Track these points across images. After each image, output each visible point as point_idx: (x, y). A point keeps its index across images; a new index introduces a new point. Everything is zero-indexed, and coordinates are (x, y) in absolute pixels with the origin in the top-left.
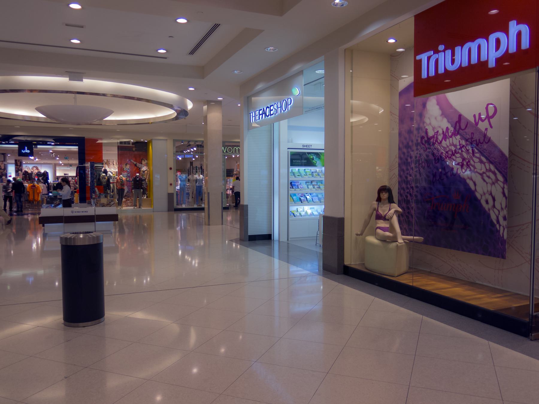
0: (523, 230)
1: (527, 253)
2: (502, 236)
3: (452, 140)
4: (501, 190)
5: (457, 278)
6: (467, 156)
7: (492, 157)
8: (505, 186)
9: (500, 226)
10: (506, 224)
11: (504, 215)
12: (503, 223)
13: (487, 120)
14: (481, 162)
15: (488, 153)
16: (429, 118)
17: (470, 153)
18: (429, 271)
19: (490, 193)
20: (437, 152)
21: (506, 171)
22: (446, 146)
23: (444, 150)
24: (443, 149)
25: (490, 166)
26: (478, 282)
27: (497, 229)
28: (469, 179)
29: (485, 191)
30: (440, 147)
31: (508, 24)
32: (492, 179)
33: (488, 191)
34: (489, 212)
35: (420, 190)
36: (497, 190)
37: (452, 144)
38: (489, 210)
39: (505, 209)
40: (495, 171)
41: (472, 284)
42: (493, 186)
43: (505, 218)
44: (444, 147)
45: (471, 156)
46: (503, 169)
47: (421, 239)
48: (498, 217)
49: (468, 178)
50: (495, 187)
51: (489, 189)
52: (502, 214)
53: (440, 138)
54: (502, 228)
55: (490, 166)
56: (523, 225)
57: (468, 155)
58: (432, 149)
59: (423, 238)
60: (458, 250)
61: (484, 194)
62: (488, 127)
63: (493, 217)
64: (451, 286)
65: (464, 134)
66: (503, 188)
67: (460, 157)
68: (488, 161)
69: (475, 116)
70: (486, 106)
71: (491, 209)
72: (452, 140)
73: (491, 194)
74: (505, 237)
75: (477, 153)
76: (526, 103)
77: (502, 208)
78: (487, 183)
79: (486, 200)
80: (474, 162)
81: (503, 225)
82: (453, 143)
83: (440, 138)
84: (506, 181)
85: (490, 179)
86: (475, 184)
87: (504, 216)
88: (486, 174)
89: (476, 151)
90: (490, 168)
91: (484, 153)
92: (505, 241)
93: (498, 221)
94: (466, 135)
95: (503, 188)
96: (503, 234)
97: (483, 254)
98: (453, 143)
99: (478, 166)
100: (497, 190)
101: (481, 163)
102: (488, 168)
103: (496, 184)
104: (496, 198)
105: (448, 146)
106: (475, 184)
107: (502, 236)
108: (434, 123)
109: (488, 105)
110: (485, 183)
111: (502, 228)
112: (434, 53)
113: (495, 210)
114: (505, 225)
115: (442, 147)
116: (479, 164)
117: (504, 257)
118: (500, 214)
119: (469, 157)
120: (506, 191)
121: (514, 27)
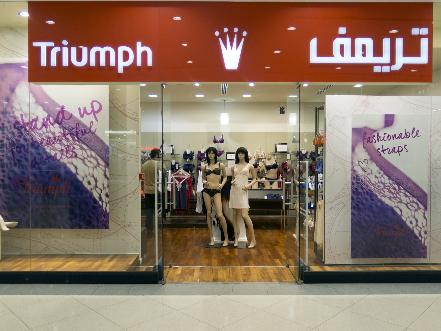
0: (118, 203)
1: (122, 221)
2: (104, 210)
3: (381, 179)
4: (103, 173)
5: (54, 254)
6: (67, 143)
7: (93, 145)
8: (107, 169)
9: (102, 202)
10: (108, 200)
11: (425, 230)
12: (106, 200)
13: (92, 114)
14: (406, 196)
15: (89, 142)
16: (19, 104)
17: (70, 140)
18: (19, 254)
19: (413, 217)
20: (367, 187)
21: (426, 202)
22: (375, 183)
23: (40, 137)
24: (372, 185)
25: (91, 152)
26: (76, 253)
27: (99, 205)
28: (70, 163)
29: (410, 215)
30: (369, 183)
31: (136, 42)
32: (415, 208)
33: (412, 215)
34: (92, 191)
35: (8, 175)
36: (99, 173)
37: (380, 182)
38: (413, 228)
39: (107, 188)
40: (417, 202)
41: (83, 257)
42: (416, 212)
43: (107, 196)
44: (373, 184)
45: (398, 192)
46: (424, 201)
47: (15, 223)
48: (100, 195)
49: (395, 207)
50: (418, 213)
51: (91, 172)
52: (104, 192)
53: (39, 125)
54: (423, 239)
55: (91, 152)
56: (118, 199)
57: (395, 191)
58: (361, 184)
59: (17, 222)
60: (59, 227)
61: (409, 217)
62: (94, 120)
63: (416, 232)
64: (62, 263)
65: (391, 176)
66: (105, 171)
67: (388, 192)
68: (89, 148)
69: (79, 109)
70: (91, 102)
71: (415, 227)
72: (381, 179)
73: (93, 176)
74: (108, 211)
75: (402, 190)
76: (118, 105)
77: (104, 188)
78: (89, 167)
79: (88, 181)
80: (400, 196)
81: (105, 201)
82: (381, 181)
83: (39, 125)
84: (107, 164)
85: (91, 164)
86: (401, 211)
87: (107, 194)
88: (87, 159)
89: (402, 188)
90: (91, 154)
91: (85, 142)
92: (108, 214)
93: (101, 198)
94: (65, 124)
95: (105, 171)
96: (106, 208)
97: (86, 228)
98: (381, 181)
99: (404, 199)
100: (99, 173)
101: (406, 197)
102: (89, 154)
103: (418, 211)
104: (98, 180)
105: (377, 183)
106: (401, 211)
107: (104, 210)
108: (26, 109)
109: (93, 102)
110: (409, 210)
111: (423, 239)
112: (56, 46)
113: (97, 189)
114: (108, 201)
115: (372, 184)
116: (404, 197)
117: (107, 227)
118: (103, 192)
119: (395, 192)
120: (108, 174)
121: (140, 48)
